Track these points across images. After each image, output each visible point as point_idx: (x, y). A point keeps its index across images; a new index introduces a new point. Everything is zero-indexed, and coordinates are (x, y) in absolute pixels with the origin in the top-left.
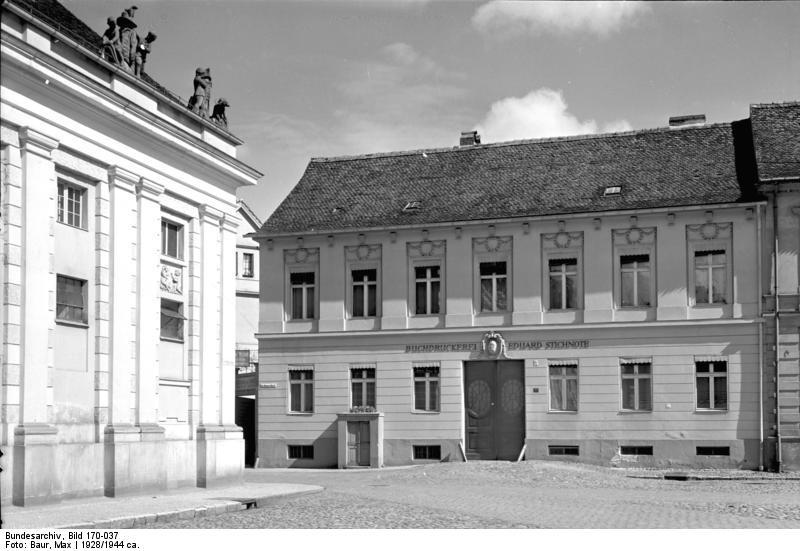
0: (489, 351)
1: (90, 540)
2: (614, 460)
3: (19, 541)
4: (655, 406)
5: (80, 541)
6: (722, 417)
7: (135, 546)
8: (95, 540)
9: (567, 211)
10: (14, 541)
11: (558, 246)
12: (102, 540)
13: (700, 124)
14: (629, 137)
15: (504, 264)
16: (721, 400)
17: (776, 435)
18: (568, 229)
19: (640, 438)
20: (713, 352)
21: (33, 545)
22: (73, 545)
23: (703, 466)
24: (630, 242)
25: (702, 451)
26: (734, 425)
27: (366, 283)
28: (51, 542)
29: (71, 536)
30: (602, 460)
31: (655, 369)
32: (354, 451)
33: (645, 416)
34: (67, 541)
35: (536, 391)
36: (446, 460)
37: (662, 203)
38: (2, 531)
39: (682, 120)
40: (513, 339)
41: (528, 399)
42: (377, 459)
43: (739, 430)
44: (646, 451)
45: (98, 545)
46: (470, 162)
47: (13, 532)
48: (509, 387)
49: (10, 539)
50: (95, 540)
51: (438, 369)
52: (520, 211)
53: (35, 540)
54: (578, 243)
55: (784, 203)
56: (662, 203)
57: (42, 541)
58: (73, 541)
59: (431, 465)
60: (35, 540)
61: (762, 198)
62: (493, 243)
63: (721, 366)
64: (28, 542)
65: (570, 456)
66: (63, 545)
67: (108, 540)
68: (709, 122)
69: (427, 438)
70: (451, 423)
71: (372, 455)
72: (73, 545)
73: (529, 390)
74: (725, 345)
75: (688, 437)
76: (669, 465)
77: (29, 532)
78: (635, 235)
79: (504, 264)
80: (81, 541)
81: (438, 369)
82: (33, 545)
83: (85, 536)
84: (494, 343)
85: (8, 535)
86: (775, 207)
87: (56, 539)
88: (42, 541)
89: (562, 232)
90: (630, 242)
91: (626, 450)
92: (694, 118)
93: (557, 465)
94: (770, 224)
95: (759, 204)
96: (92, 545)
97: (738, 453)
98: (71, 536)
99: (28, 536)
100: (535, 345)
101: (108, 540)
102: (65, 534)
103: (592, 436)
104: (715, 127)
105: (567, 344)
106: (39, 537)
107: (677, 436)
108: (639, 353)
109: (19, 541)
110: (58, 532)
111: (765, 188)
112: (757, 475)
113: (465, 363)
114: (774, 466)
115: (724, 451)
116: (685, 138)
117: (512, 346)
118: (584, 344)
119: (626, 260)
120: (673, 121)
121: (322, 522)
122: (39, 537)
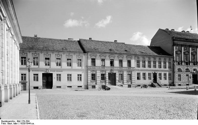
0: (47, 72)
1: (22, 122)
2: (66, 88)
3: (5, 122)
4: (72, 81)
5: (20, 123)
6: (81, 82)
7: (33, 124)
8: (24, 122)
9: (59, 51)
10: (4, 123)
11: (58, 56)
12: (25, 122)
13: (73, 40)
14: (63, 40)
15: (49, 58)
16: (81, 80)
17: (88, 84)
18: (60, 54)
19: (70, 85)
20: (80, 73)
21: (8, 124)
22: (18, 124)
23: (79, 89)
24: (68, 57)
25: (78, 87)
26: (83, 83)
27: (24, 59)
28: (13, 123)
29: (18, 121)
30: (64, 88)
31: (72, 75)
32: (22, 88)
33: (71, 82)
34: (17, 122)
35: (54, 78)
36: (40, 89)
37: (73, 52)
38: (0, 120)
39: (70, 39)
40: (51, 70)
41: (53, 79)
42: (27, 89)
43: (84, 84)
44: (71, 87)
45: (24, 124)
46: (38, 40)
47: (3, 120)
48: (50, 78)
49: (3, 122)
50: (24, 122)
51: (38, 74)
52: (52, 50)
53: (9, 122)
54: (61, 56)
55: (89, 54)
56: (73, 52)
57: (10, 123)
58: (18, 123)
59: (37, 90)
60: (9, 122)
61: (86, 53)
62: (47, 55)
63: (81, 75)
64: (7, 123)
65: (60, 88)
66: (16, 124)
67: (27, 122)
68: (74, 40)
69: (36, 86)
70: (40, 83)
71: (26, 88)
72: (18, 124)
73: (53, 78)
74: (82, 72)
75: (76, 85)
76: (74, 89)
77: (7, 120)
78: (69, 56)
79: (49, 58)
80: (20, 122)
81: (38, 74)
82: (8, 124)
83: (21, 121)
84: (48, 70)
85: (2, 121)
86: (88, 54)
87: (14, 122)
88: (10, 123)
89: (58, 54)
90: (68, 57)
91: (68, 87)
92: (72, 39)
93: (58, 89)
94: (87, 57)
95: (86, 54)
96: (23, 123)
97: (83, 87)
98: (18, 121)
99: (7, 121)
100: (54, 71)
101: (27, 122)
102: (16, 121)
103: (63, 85)
104: (75, 41)
105: (59, 71)
106: (10, 121)
107: (75, 85)
108: (70, 73)
109: (5, 122)
110: (14, 120)
111: (87, 52)
112: (86, 90)
113: (43, 73)
114: (87, 88)
115: (81, 87)
116: (71, 42)
117: (51, 71)
118: (62, 71)
119: (68, 59)
120: (68, 39)
121: (67, 118)
122: (10, 121)
